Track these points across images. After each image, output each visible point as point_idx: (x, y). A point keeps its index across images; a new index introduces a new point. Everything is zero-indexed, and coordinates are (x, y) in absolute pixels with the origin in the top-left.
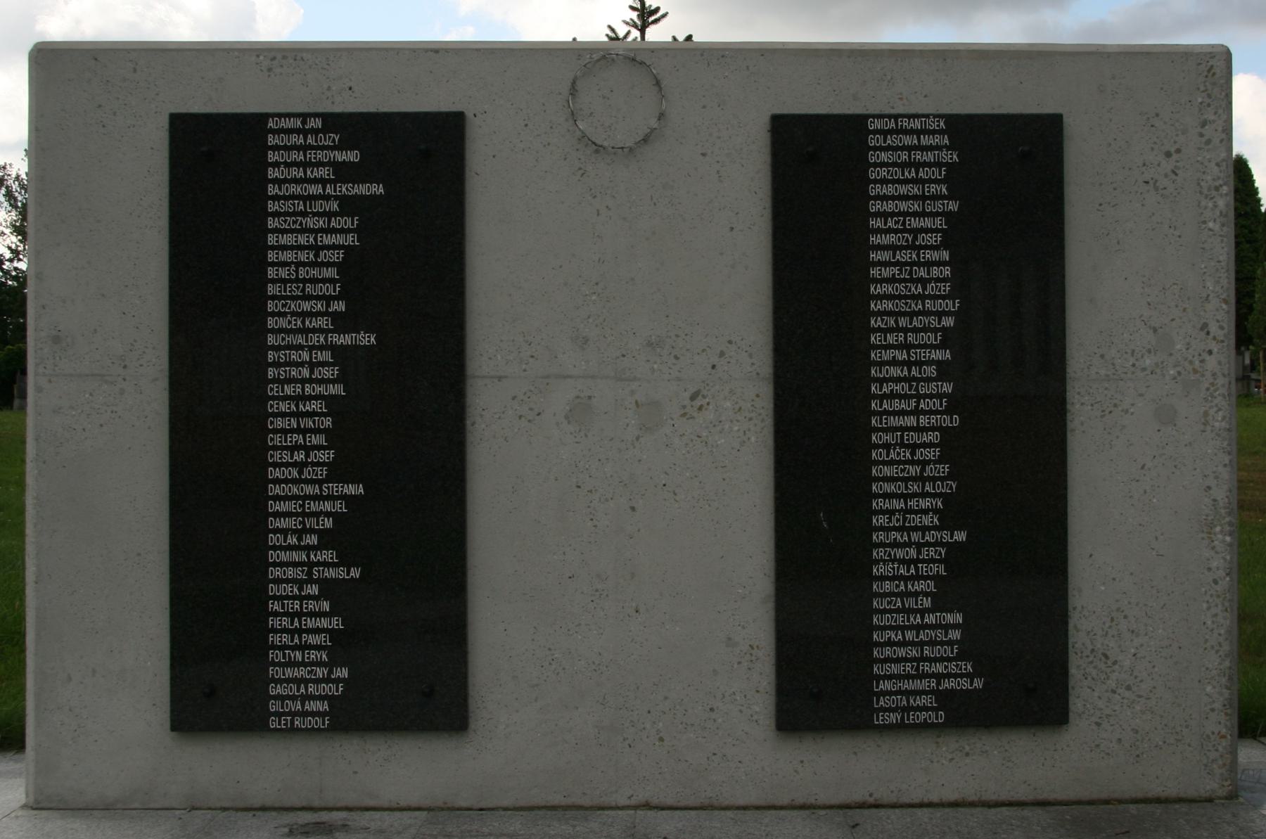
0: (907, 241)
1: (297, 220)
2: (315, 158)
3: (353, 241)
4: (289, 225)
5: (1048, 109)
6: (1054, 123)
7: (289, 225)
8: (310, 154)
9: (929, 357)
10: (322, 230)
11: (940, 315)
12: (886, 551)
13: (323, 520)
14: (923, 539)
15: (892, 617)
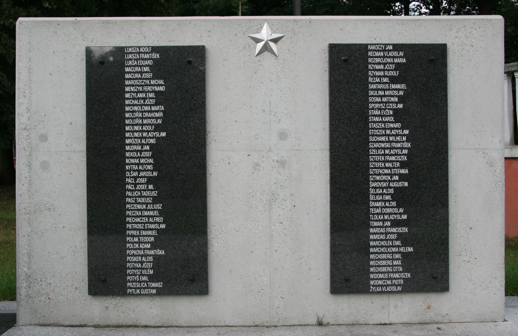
0: (382, 48)
1: (143, 81)
2: (147, 89)
3: (155, 234)
4: (140, 83)
5: (444, 43)
6: (445, 46)
7: (140, 83)
8: (145, 88)
9: (399, 172)
10: (144, 210)
11: (399, 90)
12: (371, 66)
13: (149, 271)
14: (391, 133)
15: (374, 59)
